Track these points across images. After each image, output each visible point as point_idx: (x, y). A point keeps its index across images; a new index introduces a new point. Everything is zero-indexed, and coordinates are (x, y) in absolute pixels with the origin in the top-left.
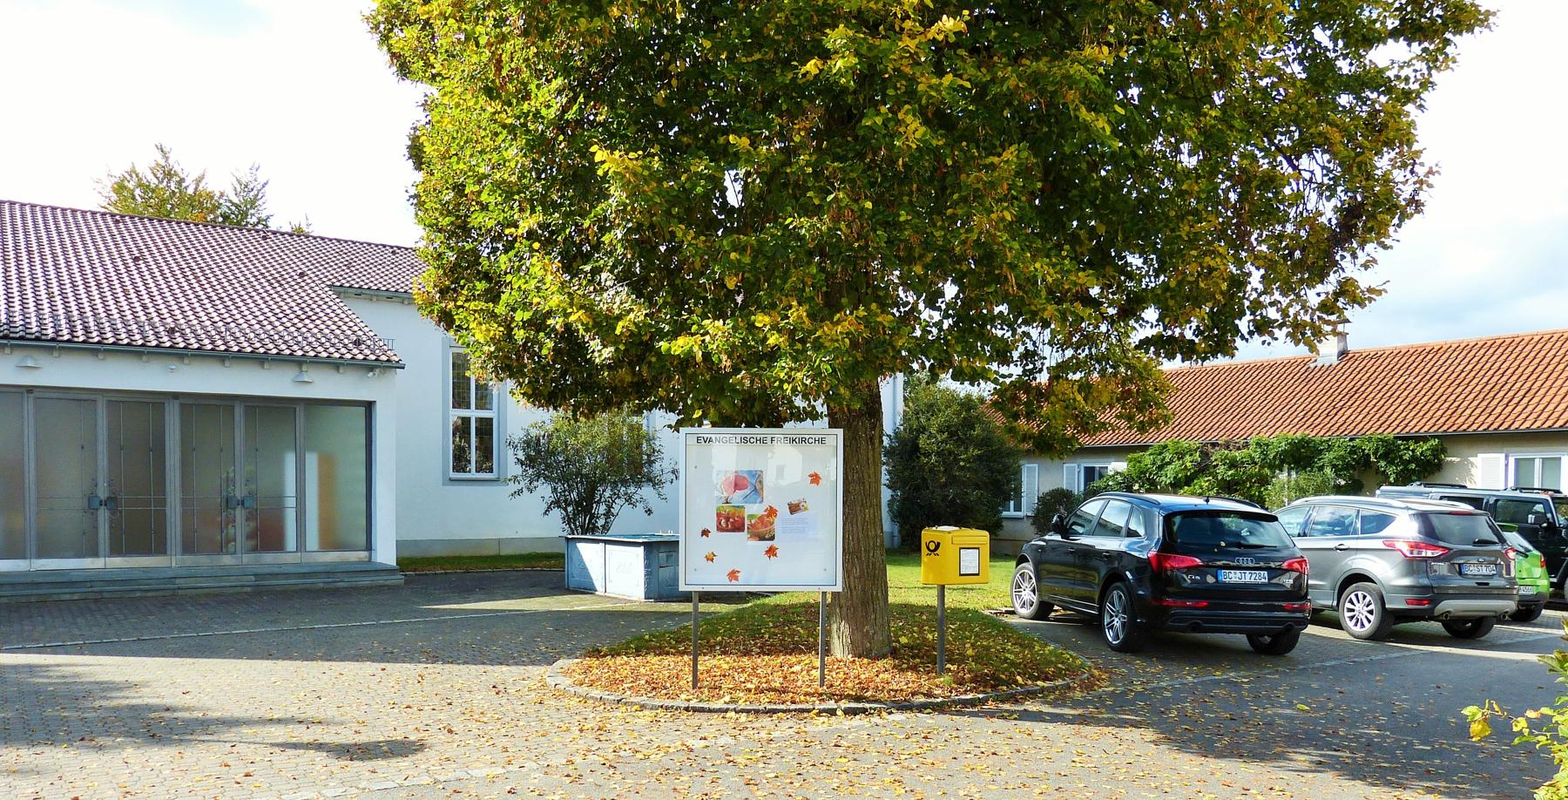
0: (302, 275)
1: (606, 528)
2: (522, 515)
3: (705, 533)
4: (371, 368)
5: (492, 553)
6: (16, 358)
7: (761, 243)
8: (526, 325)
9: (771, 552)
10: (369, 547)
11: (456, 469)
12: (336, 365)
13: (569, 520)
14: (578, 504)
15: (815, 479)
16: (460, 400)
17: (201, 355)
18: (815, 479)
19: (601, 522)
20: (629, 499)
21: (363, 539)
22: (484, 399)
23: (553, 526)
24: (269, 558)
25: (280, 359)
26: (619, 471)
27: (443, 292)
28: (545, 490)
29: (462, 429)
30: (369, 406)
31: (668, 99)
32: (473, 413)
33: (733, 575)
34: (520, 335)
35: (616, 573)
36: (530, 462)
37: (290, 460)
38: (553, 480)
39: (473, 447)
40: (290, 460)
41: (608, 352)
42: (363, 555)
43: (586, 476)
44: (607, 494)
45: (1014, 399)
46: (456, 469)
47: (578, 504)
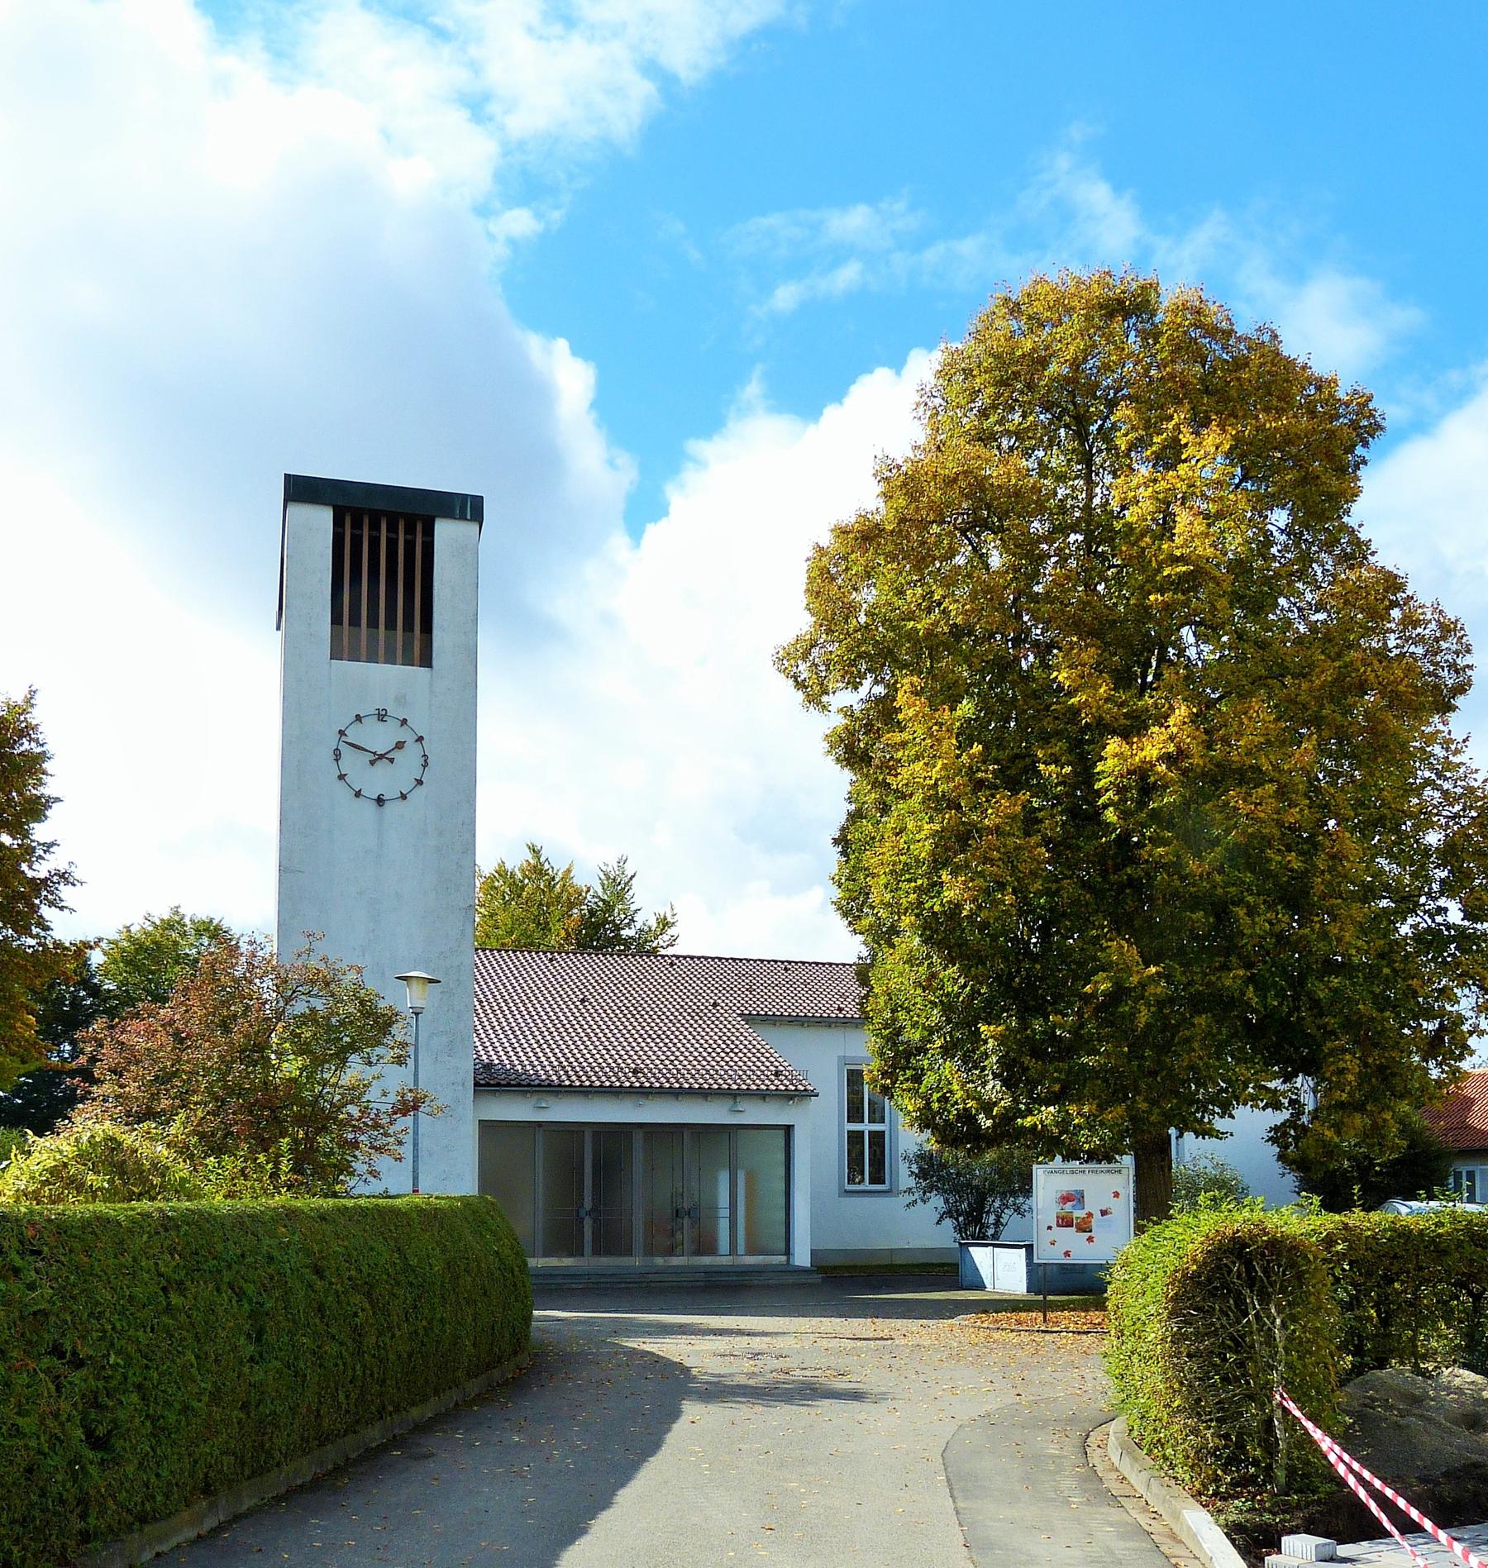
0: (715, 1005)
1: (995, 1236)
2: (914, 1223)
3: (1050, 1228)
4: (791, 1098)
5: (884, 1262)
6: (533, 1100)
7: (1071, 1068)
8: (939, 1101)
9: (1090, 1239)
10: (788, 1252)
11: (851, 1181)
12: (763, 1095)
13: (960, 1229)
14: (968, 1214)
15: (1116, 1195)
16: (855, 1114)
17: (662, 1092)
18: (1116, 1195)
19: (991, 1232)
20: (1018, 1210)
21: (782, 1245)
22: (877, 1115)
23: (944, 1236)
24: (706, 1260)
25: (720, 1094)
26: (1009, 1182)
27: (884, 1074)
28: (937, 1201)
29: (855, 1138)
30: (788, 1130)
31: (1020, 983)
32: (866, 1127)
33: (1067, 1254)
34: (935, 1106)
35: (1002, 1269)
36: (923, 1174)
37: (724, 1178)
38: (945, 1192)
39: (866, 1160)
40: (724, 1178)
41: (989, 1123)
42: (783, 1258)
43: (977, 1187)
44: (996, 1205)
45: (1285, 1134)
46: (851, 1181)
47: (968, 1214)
